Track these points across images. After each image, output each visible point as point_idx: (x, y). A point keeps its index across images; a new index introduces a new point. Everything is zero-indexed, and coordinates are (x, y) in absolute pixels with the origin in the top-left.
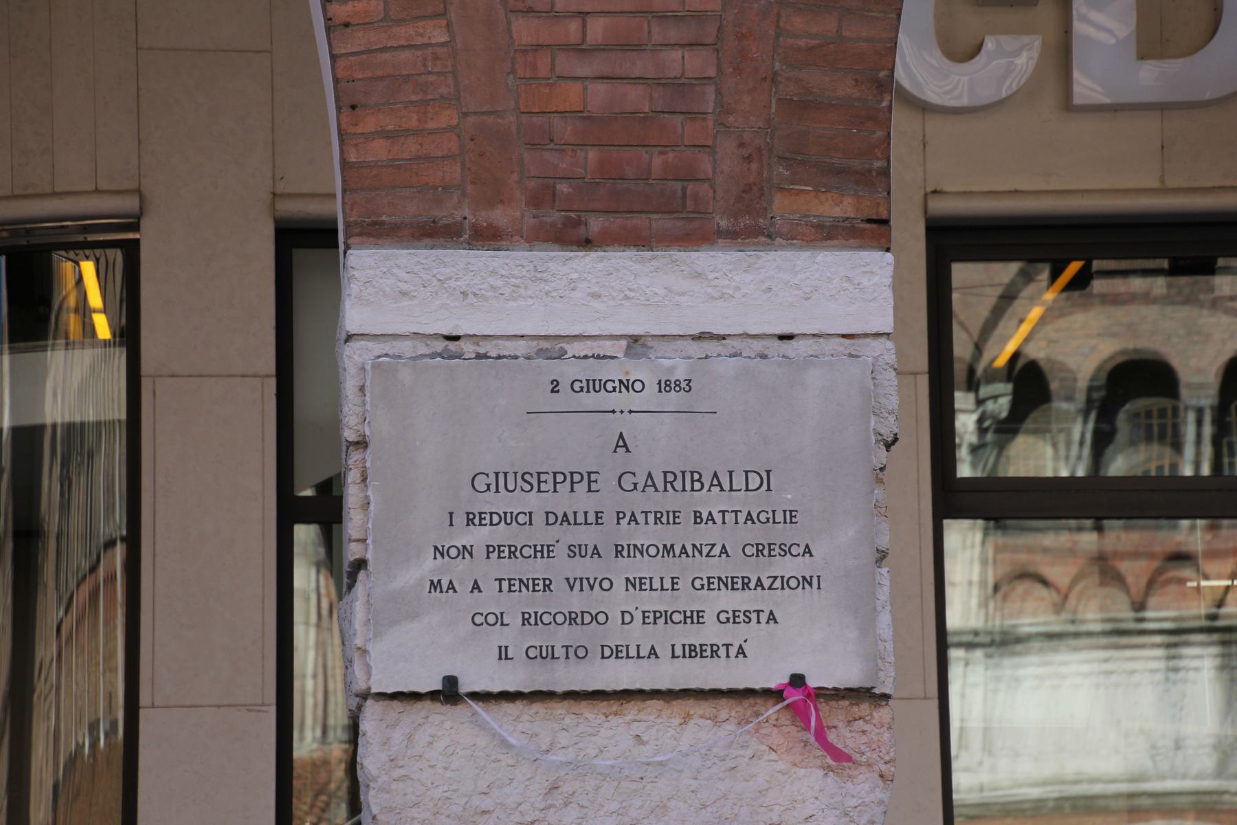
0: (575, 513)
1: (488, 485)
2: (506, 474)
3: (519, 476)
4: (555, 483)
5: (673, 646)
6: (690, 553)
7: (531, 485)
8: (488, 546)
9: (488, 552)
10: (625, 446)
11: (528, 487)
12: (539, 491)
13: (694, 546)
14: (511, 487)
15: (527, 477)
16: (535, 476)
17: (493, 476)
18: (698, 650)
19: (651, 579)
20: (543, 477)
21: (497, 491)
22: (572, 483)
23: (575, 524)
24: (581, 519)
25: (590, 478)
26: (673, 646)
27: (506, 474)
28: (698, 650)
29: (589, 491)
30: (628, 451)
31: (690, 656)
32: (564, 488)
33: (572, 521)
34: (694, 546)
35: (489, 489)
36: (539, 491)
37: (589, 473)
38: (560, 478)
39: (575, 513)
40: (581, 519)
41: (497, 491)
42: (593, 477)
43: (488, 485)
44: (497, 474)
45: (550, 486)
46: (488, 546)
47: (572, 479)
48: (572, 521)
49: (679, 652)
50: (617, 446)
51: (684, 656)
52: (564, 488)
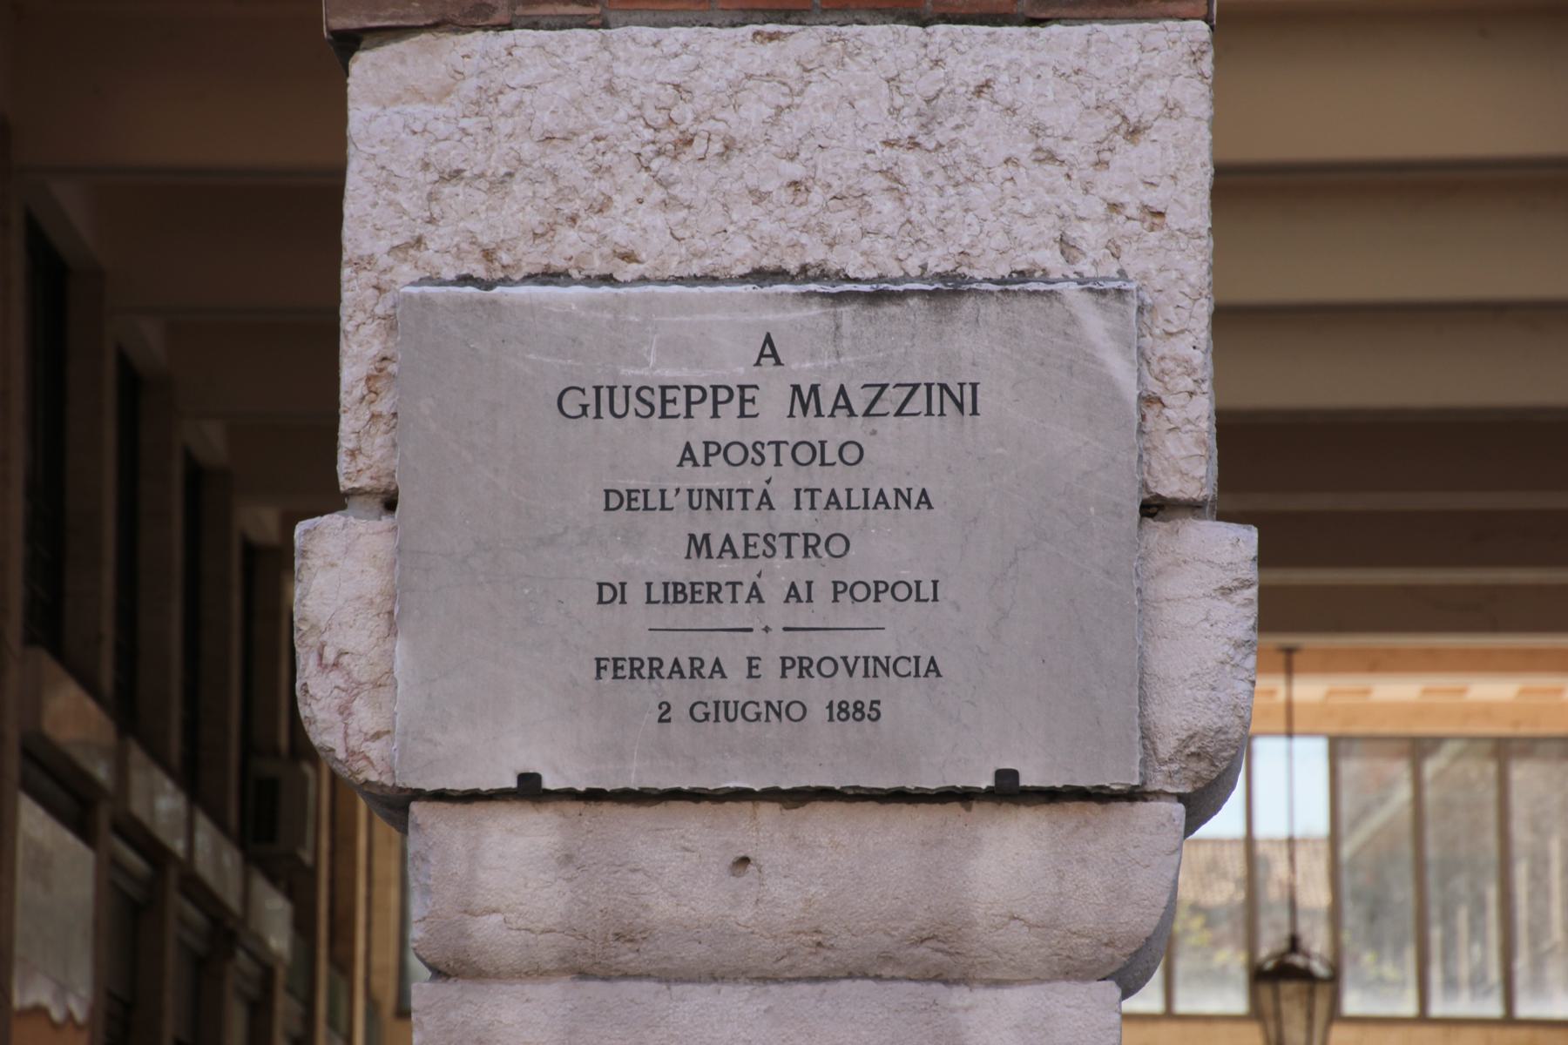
0: (849, 491)
1: (584, 407)
2: (611, 389)
3: (632, 392)
4: (689, 403)
5: (649, 585)
6: (892, 503)
7: (651, 406)
8: (783, 659)
9: (784, 668)
10: (774, 354)
11: (645, 410)
12: (664, 416)
13: (898, 491)
14: (619, 410)
15: (645, 394)
16: (658, 392)
17: (591, 393)
18: (688, 591)
19: (646, 492)
20: (670, 394)
21: (598, 416)
22: (716, 403)
23: (849, 507)
24: (857, 499)
25: (744, 395)
26: (649, 585)
27: (611, 389)
28: (688, 591)
29: (742, 415)
30: (778, 363)
31: (676, 601)
32: (703, 411)
33: (844, 503)
34: (898, 491)
35: (585, 413)
36: (664, 416)
37: (742, 388)
38: (696, 395)
39: (849, 491)
40: (857, 499)
41: (598, 416)
42: (749, 394)
43: (584, 407)
44: (598, 389)
45: (680, 408)
46: (783, 659)
47: (716, 396)
48: (844, 503)
49: (657, 593)
50: (762, 355)
51: (666, 601)
52: (703, 411)
